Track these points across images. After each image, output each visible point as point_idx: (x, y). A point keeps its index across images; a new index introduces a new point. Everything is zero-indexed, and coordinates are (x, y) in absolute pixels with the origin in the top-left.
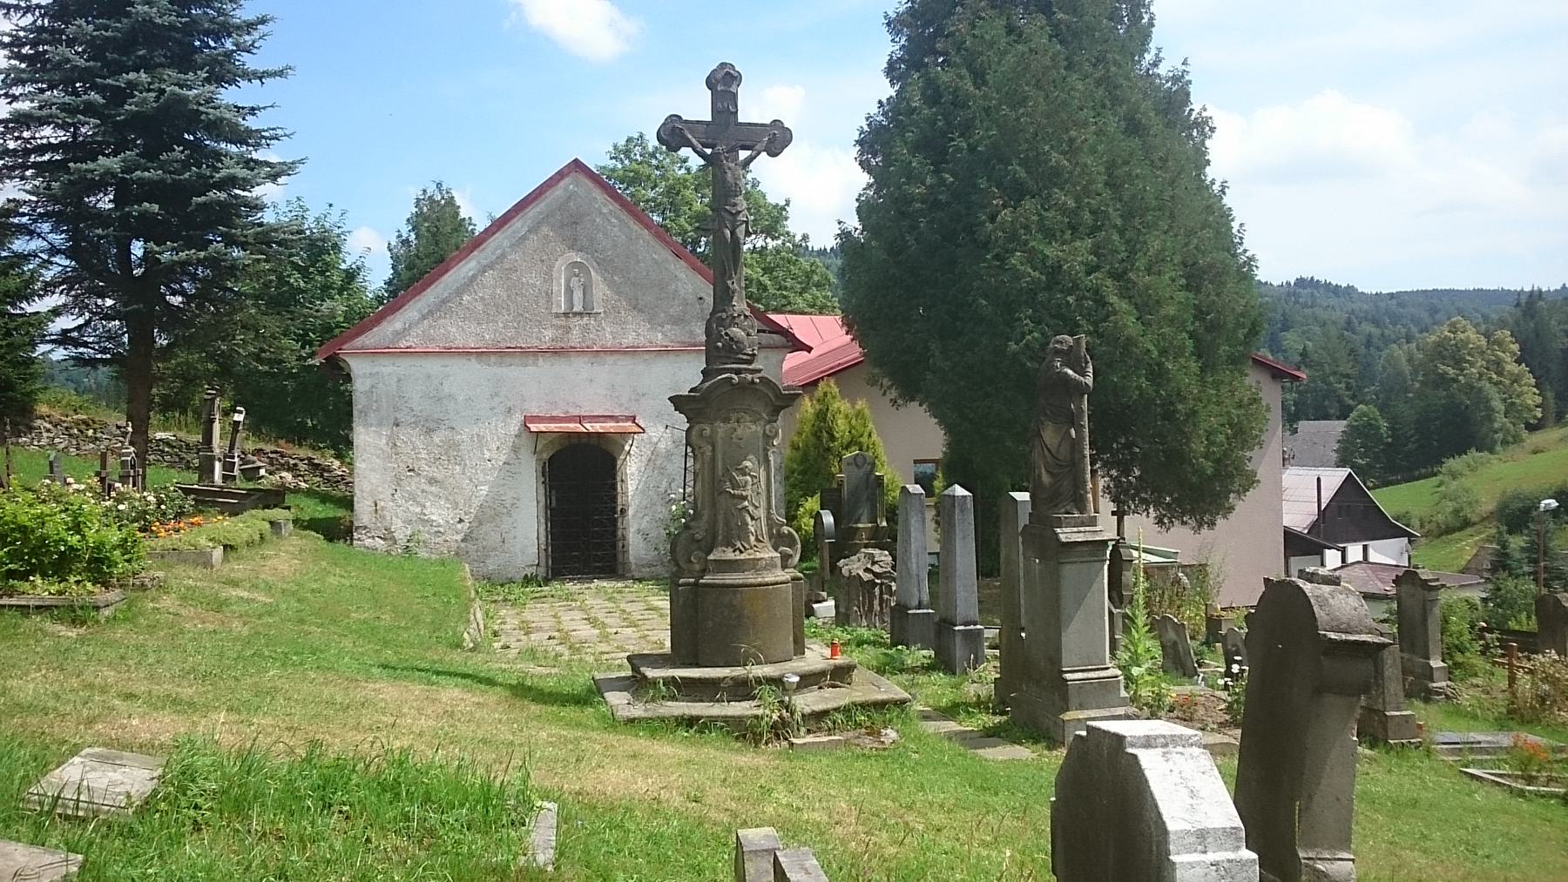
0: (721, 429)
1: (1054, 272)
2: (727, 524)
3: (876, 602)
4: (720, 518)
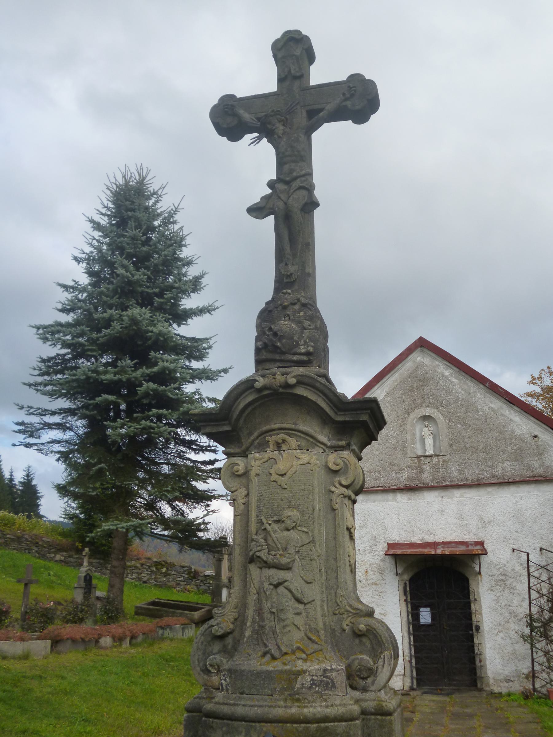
2: (259, 611)
4: (252, 599)
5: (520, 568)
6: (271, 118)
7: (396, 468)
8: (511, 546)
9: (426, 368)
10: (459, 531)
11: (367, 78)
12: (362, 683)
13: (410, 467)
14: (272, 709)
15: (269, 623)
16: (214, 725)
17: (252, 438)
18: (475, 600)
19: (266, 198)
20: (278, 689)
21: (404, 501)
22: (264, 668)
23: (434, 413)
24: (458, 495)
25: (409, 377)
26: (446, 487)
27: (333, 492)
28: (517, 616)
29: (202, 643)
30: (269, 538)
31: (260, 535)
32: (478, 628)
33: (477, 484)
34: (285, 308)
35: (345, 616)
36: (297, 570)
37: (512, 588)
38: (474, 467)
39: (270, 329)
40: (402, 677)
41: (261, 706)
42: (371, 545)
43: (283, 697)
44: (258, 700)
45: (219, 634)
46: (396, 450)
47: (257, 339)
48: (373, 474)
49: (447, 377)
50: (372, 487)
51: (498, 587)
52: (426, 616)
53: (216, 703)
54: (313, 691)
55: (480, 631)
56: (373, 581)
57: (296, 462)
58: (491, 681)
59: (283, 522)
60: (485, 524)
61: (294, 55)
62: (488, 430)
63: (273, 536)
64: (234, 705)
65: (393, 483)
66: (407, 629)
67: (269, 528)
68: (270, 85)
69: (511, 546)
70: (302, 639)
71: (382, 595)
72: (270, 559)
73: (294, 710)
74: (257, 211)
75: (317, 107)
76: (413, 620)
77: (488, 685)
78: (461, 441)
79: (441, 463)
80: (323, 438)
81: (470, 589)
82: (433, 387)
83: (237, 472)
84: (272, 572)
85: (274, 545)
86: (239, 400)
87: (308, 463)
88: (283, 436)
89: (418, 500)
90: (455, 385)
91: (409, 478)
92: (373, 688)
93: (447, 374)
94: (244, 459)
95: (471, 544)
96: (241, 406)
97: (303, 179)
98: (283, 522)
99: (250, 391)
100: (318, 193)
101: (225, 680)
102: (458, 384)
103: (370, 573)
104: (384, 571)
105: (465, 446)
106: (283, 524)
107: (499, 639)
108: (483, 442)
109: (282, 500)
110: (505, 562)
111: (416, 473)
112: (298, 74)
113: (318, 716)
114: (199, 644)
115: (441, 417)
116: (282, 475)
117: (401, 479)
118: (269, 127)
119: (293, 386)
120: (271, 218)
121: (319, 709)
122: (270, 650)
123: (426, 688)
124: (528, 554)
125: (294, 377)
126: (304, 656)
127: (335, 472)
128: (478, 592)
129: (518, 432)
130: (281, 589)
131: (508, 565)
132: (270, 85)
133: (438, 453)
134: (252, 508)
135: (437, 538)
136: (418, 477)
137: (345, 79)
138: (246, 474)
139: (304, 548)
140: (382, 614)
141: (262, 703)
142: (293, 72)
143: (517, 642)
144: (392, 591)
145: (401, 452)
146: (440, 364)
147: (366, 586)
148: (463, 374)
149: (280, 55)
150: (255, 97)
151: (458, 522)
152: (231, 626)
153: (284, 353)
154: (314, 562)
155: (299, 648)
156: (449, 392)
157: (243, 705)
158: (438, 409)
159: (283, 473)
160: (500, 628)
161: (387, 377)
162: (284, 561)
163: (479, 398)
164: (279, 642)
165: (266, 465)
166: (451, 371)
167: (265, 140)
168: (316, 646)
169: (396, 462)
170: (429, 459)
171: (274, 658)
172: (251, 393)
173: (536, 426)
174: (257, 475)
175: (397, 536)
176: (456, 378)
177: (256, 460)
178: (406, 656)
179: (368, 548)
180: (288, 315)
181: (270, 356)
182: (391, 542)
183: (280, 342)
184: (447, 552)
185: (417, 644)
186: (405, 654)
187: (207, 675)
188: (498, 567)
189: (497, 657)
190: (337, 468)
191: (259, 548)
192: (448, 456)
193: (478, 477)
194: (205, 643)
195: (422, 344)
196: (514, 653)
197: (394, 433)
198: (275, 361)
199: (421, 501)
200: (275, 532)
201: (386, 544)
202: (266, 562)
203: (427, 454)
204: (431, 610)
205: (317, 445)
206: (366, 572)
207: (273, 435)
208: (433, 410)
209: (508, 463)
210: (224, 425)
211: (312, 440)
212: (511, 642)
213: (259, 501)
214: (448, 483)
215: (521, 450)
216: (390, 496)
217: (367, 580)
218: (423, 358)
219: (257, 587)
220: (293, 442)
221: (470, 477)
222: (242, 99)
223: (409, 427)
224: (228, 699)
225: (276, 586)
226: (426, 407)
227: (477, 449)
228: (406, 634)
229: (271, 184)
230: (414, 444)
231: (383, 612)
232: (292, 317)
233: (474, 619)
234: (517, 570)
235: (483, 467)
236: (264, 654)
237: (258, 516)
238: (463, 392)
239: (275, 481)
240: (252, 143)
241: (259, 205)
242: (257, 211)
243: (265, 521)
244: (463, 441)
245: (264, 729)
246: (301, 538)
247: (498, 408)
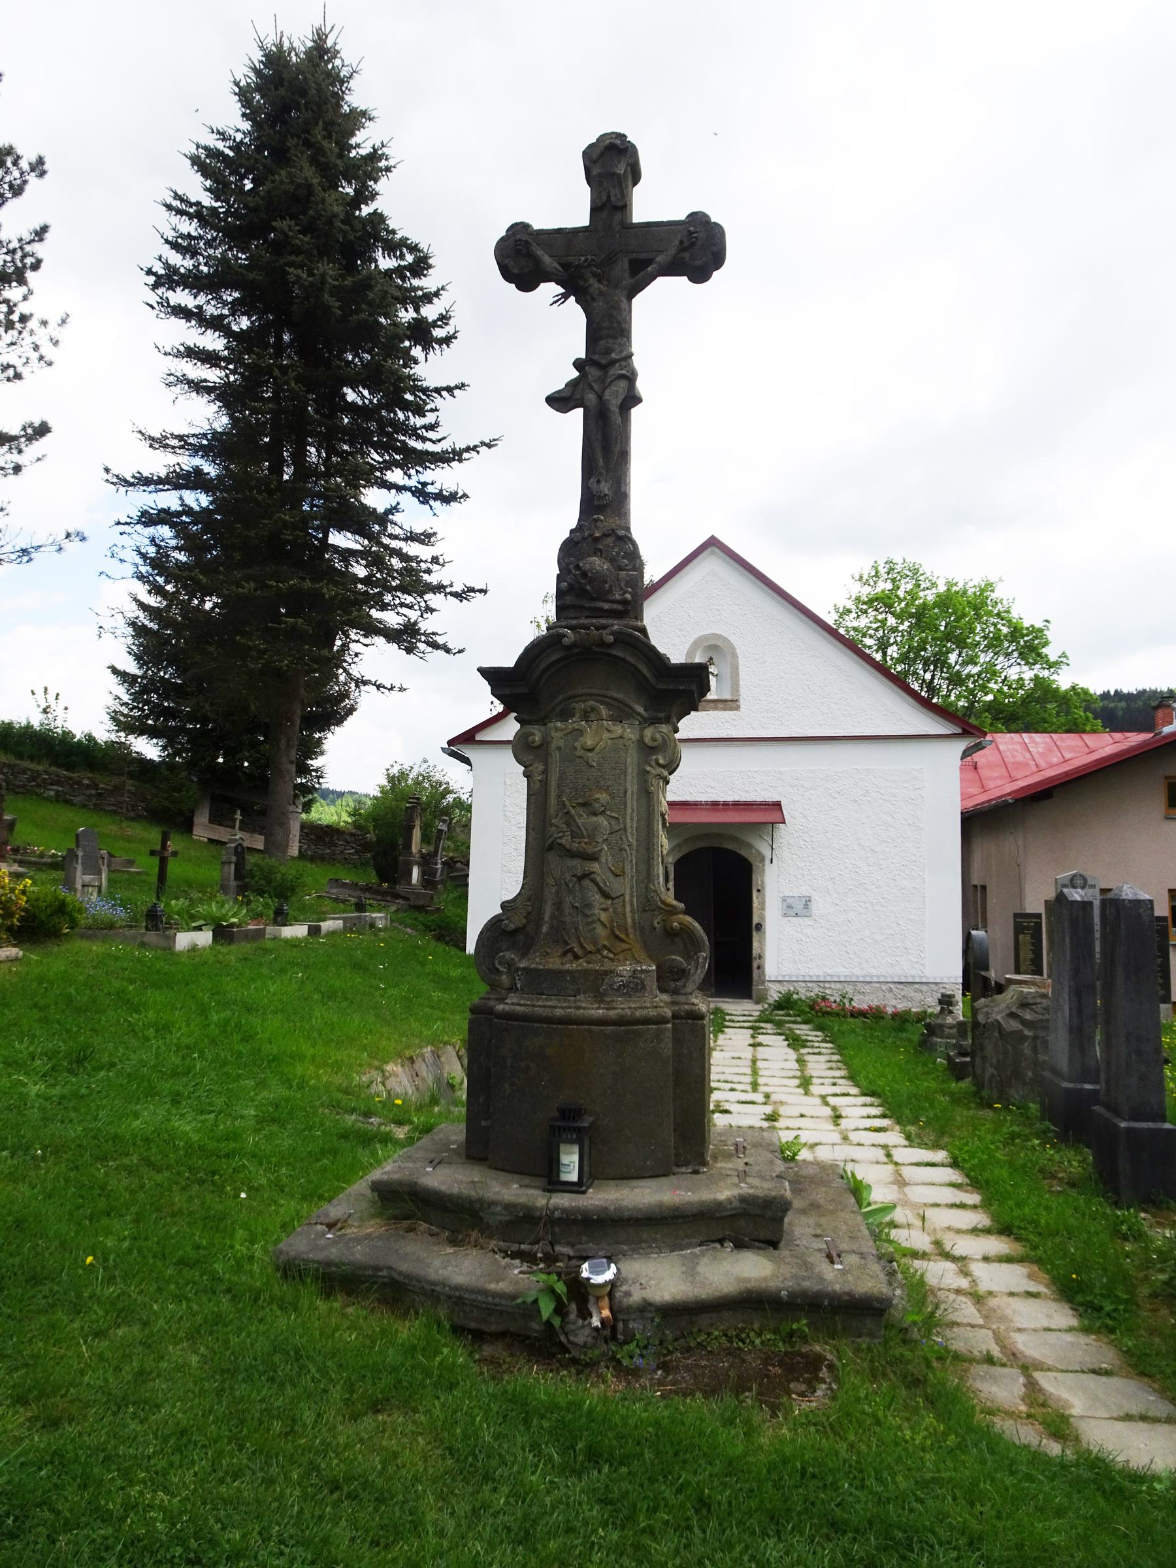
2: (559, 905)
4: (550, 892)
11: (713, 220)
12: (672, 985)
19: (573, 384)
22: (567, 966)
32: (759, 927)
39: (577, 567)
45: (509, 929)
47: (559, 578)
57: (606, 735)
61: (615, 174)
67: (573, 812)
68: (582, 219)
74: (559, 402)
75: (643, 256)
80: (640, 709)
84: (576, 862)
88: (591, 703)
94: (542, 728)
96: (543, 666)
97: (623, 363)
100: (641, 385)
112: (620, 204)
118: (581, 283)
119: (610, 646)
120: (579, 412)
126: (611, 955)
130: (586, 882)
132: (582, 219)
137: (683, 218)
138: (545, 744)
142: (613, 199)
149: (595, 171)
150: (559, 231)
152: (524, 921)
155: (605, 947)
162: (590, 850)
167: (572, 298)
168: (625, 946)
171: (576, 957)
174: (559, 748)
177: (557, 729)
190: (655, 744)
195: (713, 543)
202: (569, 851)
213: (560, 779)
222: (542, 233)
225: (581, 878)
229: (578, 364)
236: (565, 954)
237: (558, 797)
240: (555, 302)
241: (563, 395)
242: (559, 402)
243: (567, 803)
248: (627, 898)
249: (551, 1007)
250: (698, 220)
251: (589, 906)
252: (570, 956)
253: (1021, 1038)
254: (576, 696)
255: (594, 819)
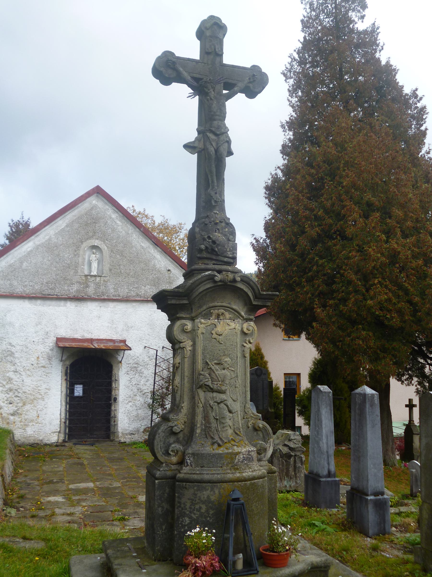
0: (202, 324)
1: (394, 257)
2: (206, 417)
3: (291, 469)
4: (200, 410)
5: (148, 359)
6: (208, 84)
7: (68, 282)
8: (144, 344)
9: (98, 209)
10: (110, 332)
13: (79, 283)
14: (225, 475)
15: (214, 424)
16: (187, 486)
17: (202, 309)
18: (116, 380)
20: (225, 463)
21: (72, 307)
23: (101, 245)
24: (112, 307)
25: (86, 215)
26: (104, 300)
27: (245, 346)
28: (142, 391)
29: (163, 437)
30: (213, 374)
31: (205, 371)
32: (115, 399)
33: (126, 300)
34: (216, 224)
35: (249, 420)
36: (229, 394)
37: (141, 373)
38: (125, 287)
39: (209, 238)
40: (57, 433)
41: (218, 474)
42: (43, 338)
43: (228, 468)
44: (215, 470)
46: (70, 268)
48: (50, 285)
49: (113, 219)
50: (48, 295)
51: (132, 372)
52: (79, 390)
53: (185, 473)
54: (244, 463)
55: (117, 401)
56: (42, 365)
57: (227, 328)
58: (120, 435)
59: (222, 364)
60: (128, 328)
62: (137, 262)
63: (216, 373)
64: (200, 474)
65: (65, 293)
66: (65, 400)
67: (213, 368)
69: (144, 344)
70: (232, 434)
71: (49, 375)
72: (215, 387)
73: (238, 475)
74: (188, 147)
76: (69, 393)
77: (118, 437)
78: (118, 267)
79: (102, 282)
80: (243, 314)
81: (113, 372)
82: (102, 225)
83: (186, 330)
84: (215, 394)
85: (216, 378)
86: (200, 286)
87: (235, 328)
88: (223, 311)
89: (83, 308)
90: (119, 226)
91: (78, 291)
92: (264, 459)
93: (114, 217)
95: (117, 342)
96: (201, 289)
98: (222, 364)
99: (207, 282)
101: (189, 460)
102: (121, 226)
103: (41, 359)
104: (52, 358)
105: (121, 272)
106: (222, 366)
107: (128, 406)
108: (133, 270)
109: (219, 350)
110: (138, 355)
111: (83, 287)
113: (251, 477)
114: (161, 438)
115: (106, 248)
116: (220, 335)
117: (71, 291)
121: (250, 473)
122: (217, 441)
123: (74, 441)
124: (157, 351)
125: (239, 277)
127: (245, 334)
128: (118, 375)
129: (158, 266)
130: (222, 405)
131: (140, 357)
133: (100, 274)
134: (198, 354)
135: (93, 336)
136: (84, 290)
139: (232, 380)
140: (47, 389)
141: (218, 472)
143: (140, 409)
144: (56, 372)
145: (73, 271)
146: (110, 209)
147: (37, 369)
148: (126, 219)
150: (189, 59)
151: (110, 325)
153: (217, 255)
154: (237, 389)
155: (232, 439)
156: (113, 230)
157: (207, 474)
158: (104, 242)
159: (221, 334)
160: (130, 399)
161: (69, 212)
162: (223, 388)
163: (134, 238)
164: (221, 436)
165: (209, 328)
166: (117, 215)
169: (69, 277)
170: (93, 278)
171: (219, 445)
172: (209, 283)
173: (170, 263)
174: (203, 333)
175: (64, 333)
176: (119, 221)
177: (201, 323)
178: (63, 419)
179: (41, 340)
180: (218, 229)
181: (209, 256)
182: (59, 337)
183: (217, 248)
184: (102, 346)
185: (72, 410)
186: (62, 417)
187: (167, 456)
188: (134, 358)
189: (126, 418)
191: (207, 380)
192: (108, 278)
193: (127, 295)
194: (164, 437)
195: (98, 191)
196: (137, 416)
197: (69, 256)
198: (211, 259)
199: (85, 308)
200: (217, 370)
201: (55, 338)
203: (92, 274)
204: (84, 386)
205: (239, 318)
206: (38, 358)
207: (216, 309)
208: (100, 242)
209: (149, 287)
210: (185, 299)
211: (237, 314)
212: (136, 408)
213: (204, 350)
214: (106, 297)
215: (159, 279)
216: (62, 303)
217: (38, 364)
218: (97, 202)
219: (203, 403)
220: (227, 315)
221: (121, 294)
222: (179, 58)
223: (81, 252)
224: (194, 471)
226: (96, 239)
227: (128, 275)
228: (64, 404)
230: (84, 266)
231: (48, 387)
232: (221, 231)
233: (113, 393)
234: (146, 361)
235: (131, 288)
236: (213, 444)
238: (124, 232)
239: (215, 338)
240: (190, 96)
244: (120, 268)
245: (223, 487)
246: (231, 374)
247: (147, 247)
248: (239, 413)
249: (212, 474)
250: (256, 69)
251: (223, 418)
252: (216, 446)
253: (290, 456)
254: (213, 307)
255: (223, 371)
